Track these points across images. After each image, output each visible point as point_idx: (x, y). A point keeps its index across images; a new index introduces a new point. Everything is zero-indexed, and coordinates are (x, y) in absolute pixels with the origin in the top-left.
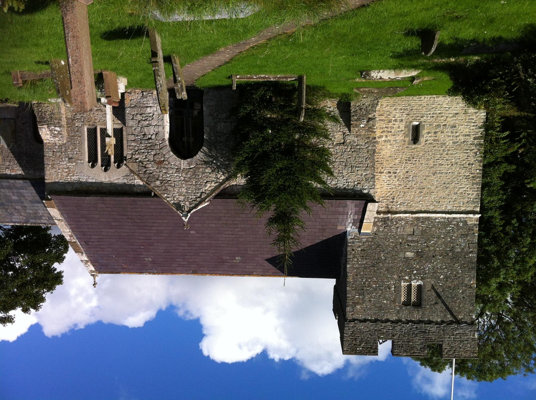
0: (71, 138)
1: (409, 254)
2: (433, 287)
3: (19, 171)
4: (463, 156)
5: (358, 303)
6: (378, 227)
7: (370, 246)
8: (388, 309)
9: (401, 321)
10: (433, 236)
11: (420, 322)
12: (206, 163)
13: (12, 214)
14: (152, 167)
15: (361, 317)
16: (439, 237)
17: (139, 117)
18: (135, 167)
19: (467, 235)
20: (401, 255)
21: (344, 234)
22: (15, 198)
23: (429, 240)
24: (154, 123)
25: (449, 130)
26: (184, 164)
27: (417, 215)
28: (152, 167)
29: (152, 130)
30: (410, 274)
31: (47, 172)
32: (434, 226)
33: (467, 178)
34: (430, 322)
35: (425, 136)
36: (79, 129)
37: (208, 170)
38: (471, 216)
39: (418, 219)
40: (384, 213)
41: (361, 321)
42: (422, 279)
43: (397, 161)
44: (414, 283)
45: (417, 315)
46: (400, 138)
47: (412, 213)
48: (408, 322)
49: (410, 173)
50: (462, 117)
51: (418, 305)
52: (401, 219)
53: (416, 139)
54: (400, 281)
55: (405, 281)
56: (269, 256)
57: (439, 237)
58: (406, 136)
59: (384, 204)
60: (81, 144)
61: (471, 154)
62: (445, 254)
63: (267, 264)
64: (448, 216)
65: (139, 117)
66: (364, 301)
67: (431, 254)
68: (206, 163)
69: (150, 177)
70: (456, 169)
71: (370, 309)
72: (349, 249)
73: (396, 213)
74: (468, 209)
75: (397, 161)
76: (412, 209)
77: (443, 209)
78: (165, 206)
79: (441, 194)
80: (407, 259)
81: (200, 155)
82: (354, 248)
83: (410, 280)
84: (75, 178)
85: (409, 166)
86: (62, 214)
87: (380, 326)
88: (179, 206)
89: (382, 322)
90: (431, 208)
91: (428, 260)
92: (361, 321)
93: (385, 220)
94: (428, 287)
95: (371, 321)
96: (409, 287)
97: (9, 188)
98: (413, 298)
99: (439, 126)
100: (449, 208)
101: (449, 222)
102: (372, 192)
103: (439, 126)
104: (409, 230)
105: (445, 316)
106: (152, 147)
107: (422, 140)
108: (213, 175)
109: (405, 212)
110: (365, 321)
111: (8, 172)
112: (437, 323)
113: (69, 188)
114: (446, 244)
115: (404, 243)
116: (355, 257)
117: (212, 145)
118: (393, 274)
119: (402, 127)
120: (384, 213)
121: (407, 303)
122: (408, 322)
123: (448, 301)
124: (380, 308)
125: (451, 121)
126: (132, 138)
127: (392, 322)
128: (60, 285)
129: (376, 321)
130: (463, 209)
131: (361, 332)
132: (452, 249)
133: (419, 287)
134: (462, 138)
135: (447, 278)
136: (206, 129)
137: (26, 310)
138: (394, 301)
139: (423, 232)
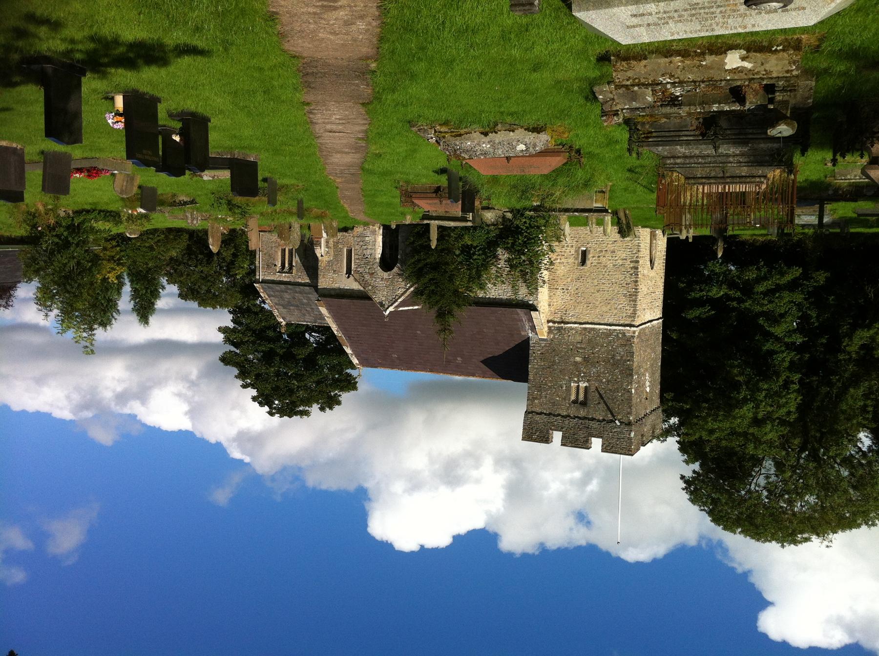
0: (335, 256)
1: (578, 359)
2: (597, 389)
3: (308, 281)
4: (621, 277)
5: (536, 398)
6: (554, 335)
7: (547, 351)
8: (560, 405)
9: (569, 416)
10: (597, 344)
11: (585, 418)
12: (399, 275)
13: (304, 315)
14: (367, 277)
15: (538, 410)
16: (602, 346)
17: (361, 243)
18: (357, 276)
19: (625, 345)
20: (572, 360)
21: (528, 339)
22: (305, 301)
23: (593, 348)
24: (370, 247)
25: (609, 254)
26: (386, 275)
27: (584, 326)
28: (367, 277)
29: (369, 252)
30: (578, 376)
31: (320, 281)
32: (598, 336)
33: (625, 295)
34: (593, 419)
35: (590, 260)
36: (341, 250)
37: (400, 280)
38: (628, 328)
39: (585, 329)
40: (559, 323)
41: (538, 414)
42: (588, 381)
43: (569, 280)
44: (583, 385)
45: (582, 413)
46: (571, 260)
47: (581, 323)
48: (575, 417)
49: (580, 291)
50: (620, 244)
51: (584, 404)
52: (572, 329)
53: (583, 262)
54: (570, 382)
55: (575, 382)
56: (482, 358)
57: (602, 346)
58: (576, 259)
59: (559, 316)
60: (342, 261)
61: (628, 275)
62: (607, 361)
63: (483, 366)
64: (609, 328)
65: (361, 243)
66: (541, 397)
67: (596, 360)
68: (399, 275)
69: (365, 284)
70: (617, 288)
71: (546, 404)
72: (531, 352)
73: (568, 323)
74: (626, 322)
75: (569, 280)
76: (579, 321)
77: (606, 321)
78: (374, 304)
79: (604, 309)
80: (576, 362)
81: (396, 269)
82: (535, 352)
83: (578, 382)
84: (336, 286)
85: (578, 284)
86: (330, 313)
87: (552, 419)
88: (381, 304)
89: (554, 415)
90: (596, 320)
91: (593, 365)
92: (538, 414)
93: (559, 329)
94: (593, 389)
95: (545, 414)
96: (578, 387)
97: (300, 293)
98: (581, 397)
99: (601, 251)
100: (611, 321)
101: (610, 333)
102: (535, 303)
103: (601, 251)
104: (579, 338)
105: (606, 415)
106: (367, 264)
107: (588, 262)
108: (403, 283)
109: (575, 323)
110: (541, 413)
111: (300, 280)
112: (599, 421)
113: (333, 293)
114: (608, 352)
115: (575, 349)
116: (535, 359)
117: (403, 263)
118: (565, 375)
119: (573, 252)
120: (559, 323)
121: (575, 402)
122: (575, 417)
123: (609, 402)
124: (554, 404)
125: (611, 247)
126: (357, 257)
127: (563, 416)
128: (352, 392)
129: (550, 414)
130: (622, 322)
131: (537, 423)
132: (613, 357)
133: (586, 387)
134: (621, 262)
135: (608, 381)
136: (400, 252)
137: (322, 409)
138: (565, 399)
139: (590, 341)
